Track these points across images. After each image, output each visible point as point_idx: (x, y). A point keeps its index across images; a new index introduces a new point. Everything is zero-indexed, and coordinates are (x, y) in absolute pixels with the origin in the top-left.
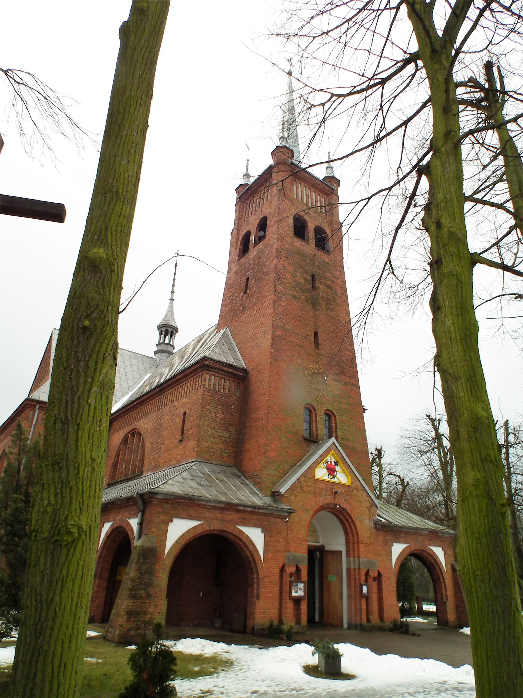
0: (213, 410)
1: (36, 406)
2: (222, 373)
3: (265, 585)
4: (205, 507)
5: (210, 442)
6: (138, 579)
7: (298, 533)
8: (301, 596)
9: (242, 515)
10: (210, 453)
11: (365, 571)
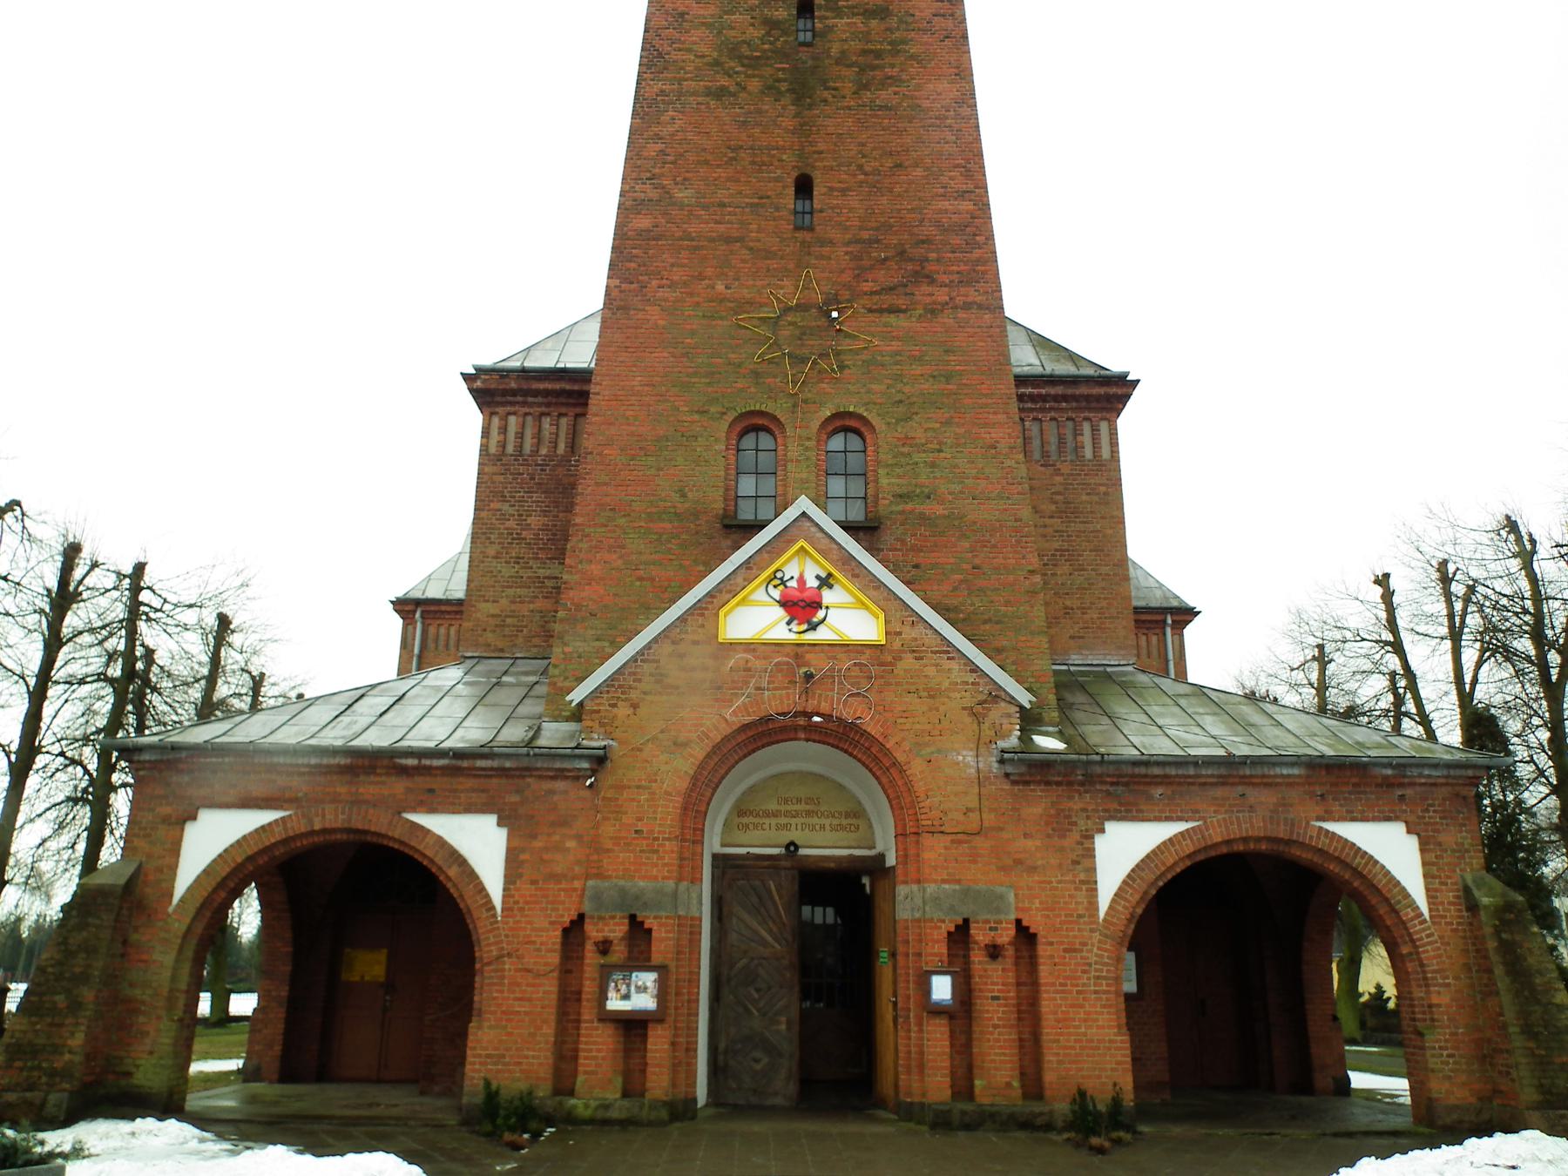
0: (511, 511)
1: (414, 612)
2: (540, 399)
3: (503, 977)
5: (504, 602)
6: (52, 966)
8: (646, 1012)
9: (421, 782)
10: (507, 631)
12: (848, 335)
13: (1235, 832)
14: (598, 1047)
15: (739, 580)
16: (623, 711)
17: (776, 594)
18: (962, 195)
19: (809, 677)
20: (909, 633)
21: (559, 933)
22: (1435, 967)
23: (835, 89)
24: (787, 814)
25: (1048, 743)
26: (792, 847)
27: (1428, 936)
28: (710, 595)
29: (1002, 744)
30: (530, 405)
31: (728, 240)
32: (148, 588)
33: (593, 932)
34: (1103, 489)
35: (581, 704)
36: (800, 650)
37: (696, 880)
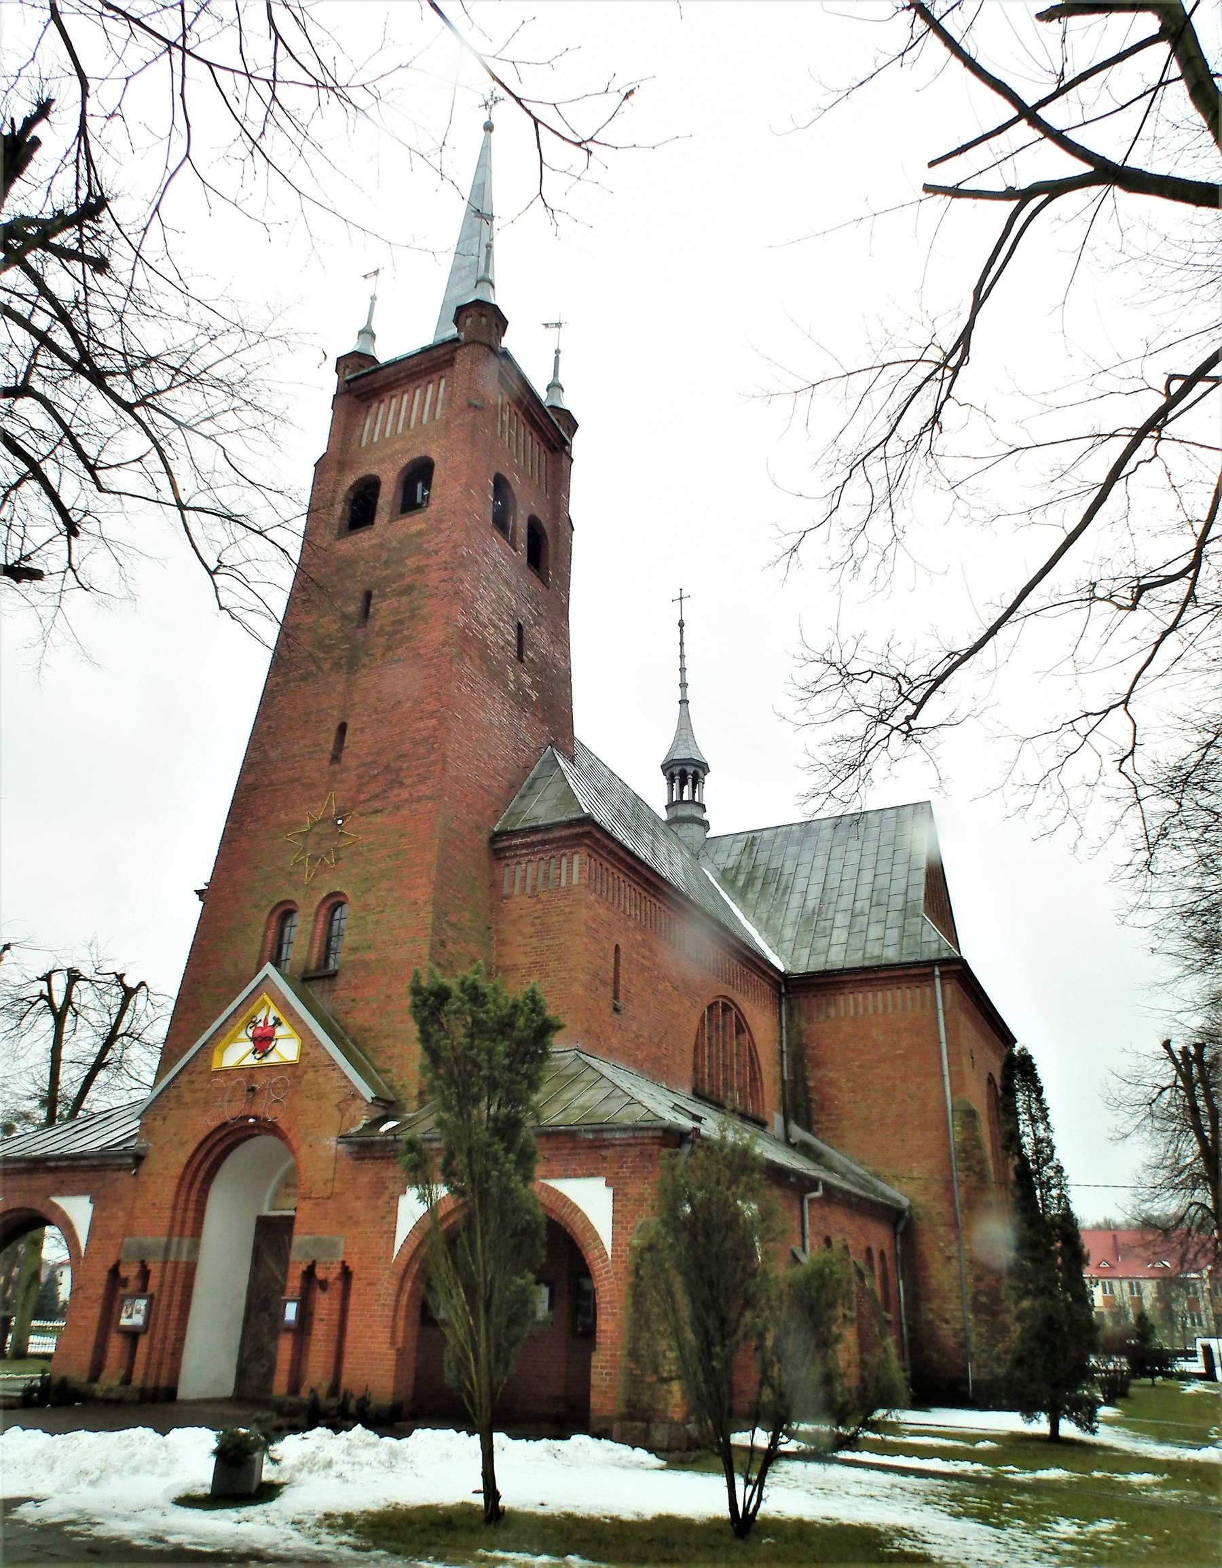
9: (60, 1176)
11: (303, 1267)
17: (250, 1033)
20: (314, 1053)
22: (608, 1299)
27: (607, 1272)
28: (211, 1038)
34: (568, 910)
36: (253, 1071)
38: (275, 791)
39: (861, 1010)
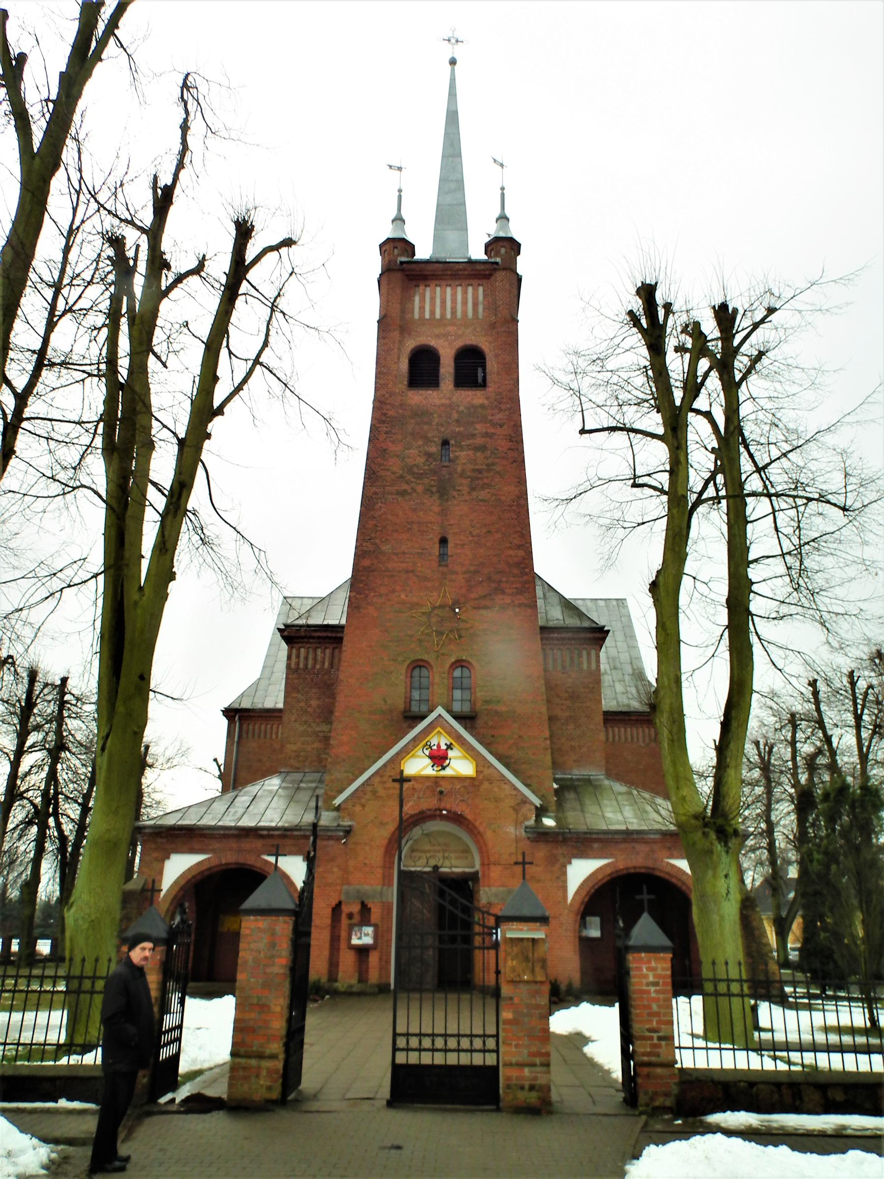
0: (302, 698)
4: (212, 837)
7: (366, 858)
12: (464, 621)
13: (630, 864)
14: (347, 960)
15: (411, 747)
16: (358, 808)
17: (427, 752)
18: (519, 547)
19: (441, 792)
20: (487, 772)
21: (330, 910)
23: (459, 490)
24: (435, 851)
25: (549, 822)
26: (436, 868)
29: (527, 823)
30: (311, 643)
31: (407, 572)
32: (70, 693)
33: (345, 909)
35: (339, 805)
37: (390, 884)
38: (392, 576)
39: (617, 738)
